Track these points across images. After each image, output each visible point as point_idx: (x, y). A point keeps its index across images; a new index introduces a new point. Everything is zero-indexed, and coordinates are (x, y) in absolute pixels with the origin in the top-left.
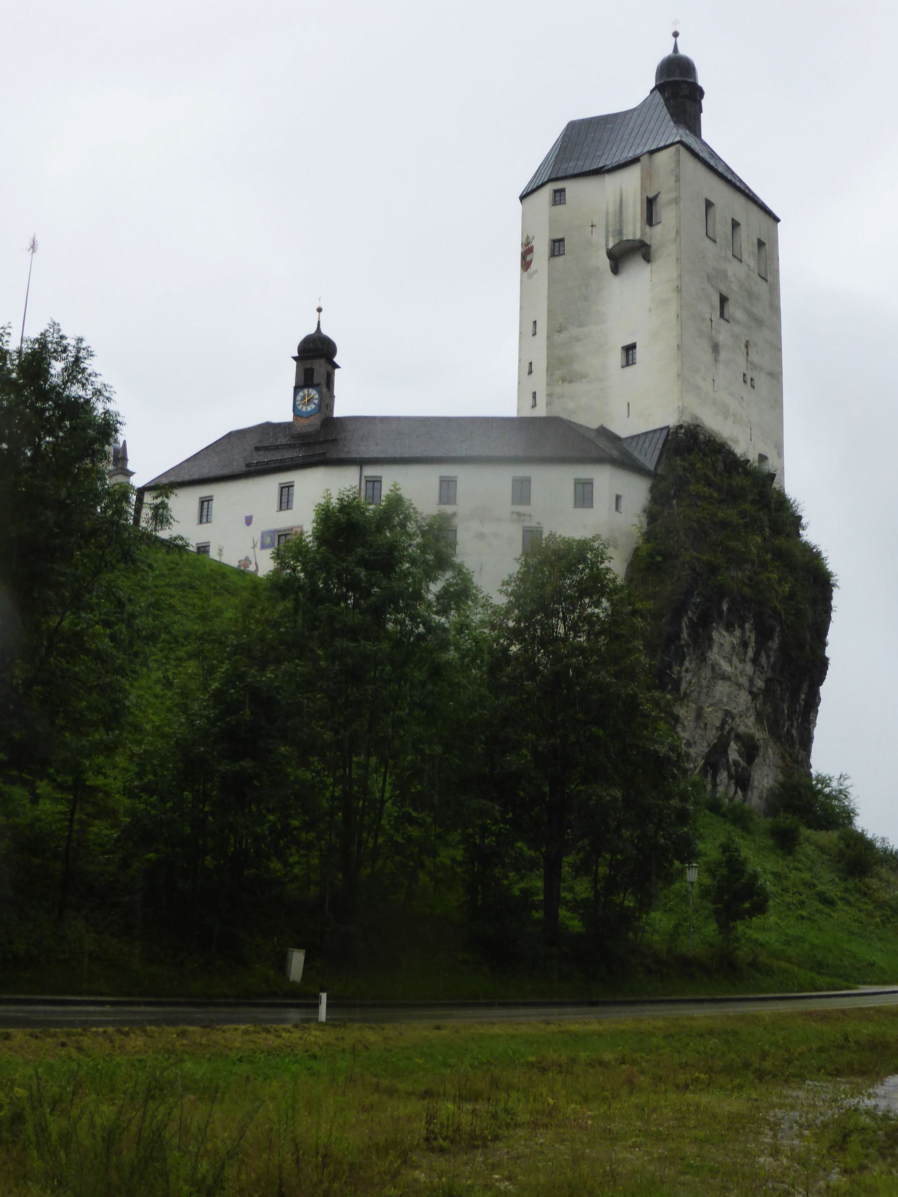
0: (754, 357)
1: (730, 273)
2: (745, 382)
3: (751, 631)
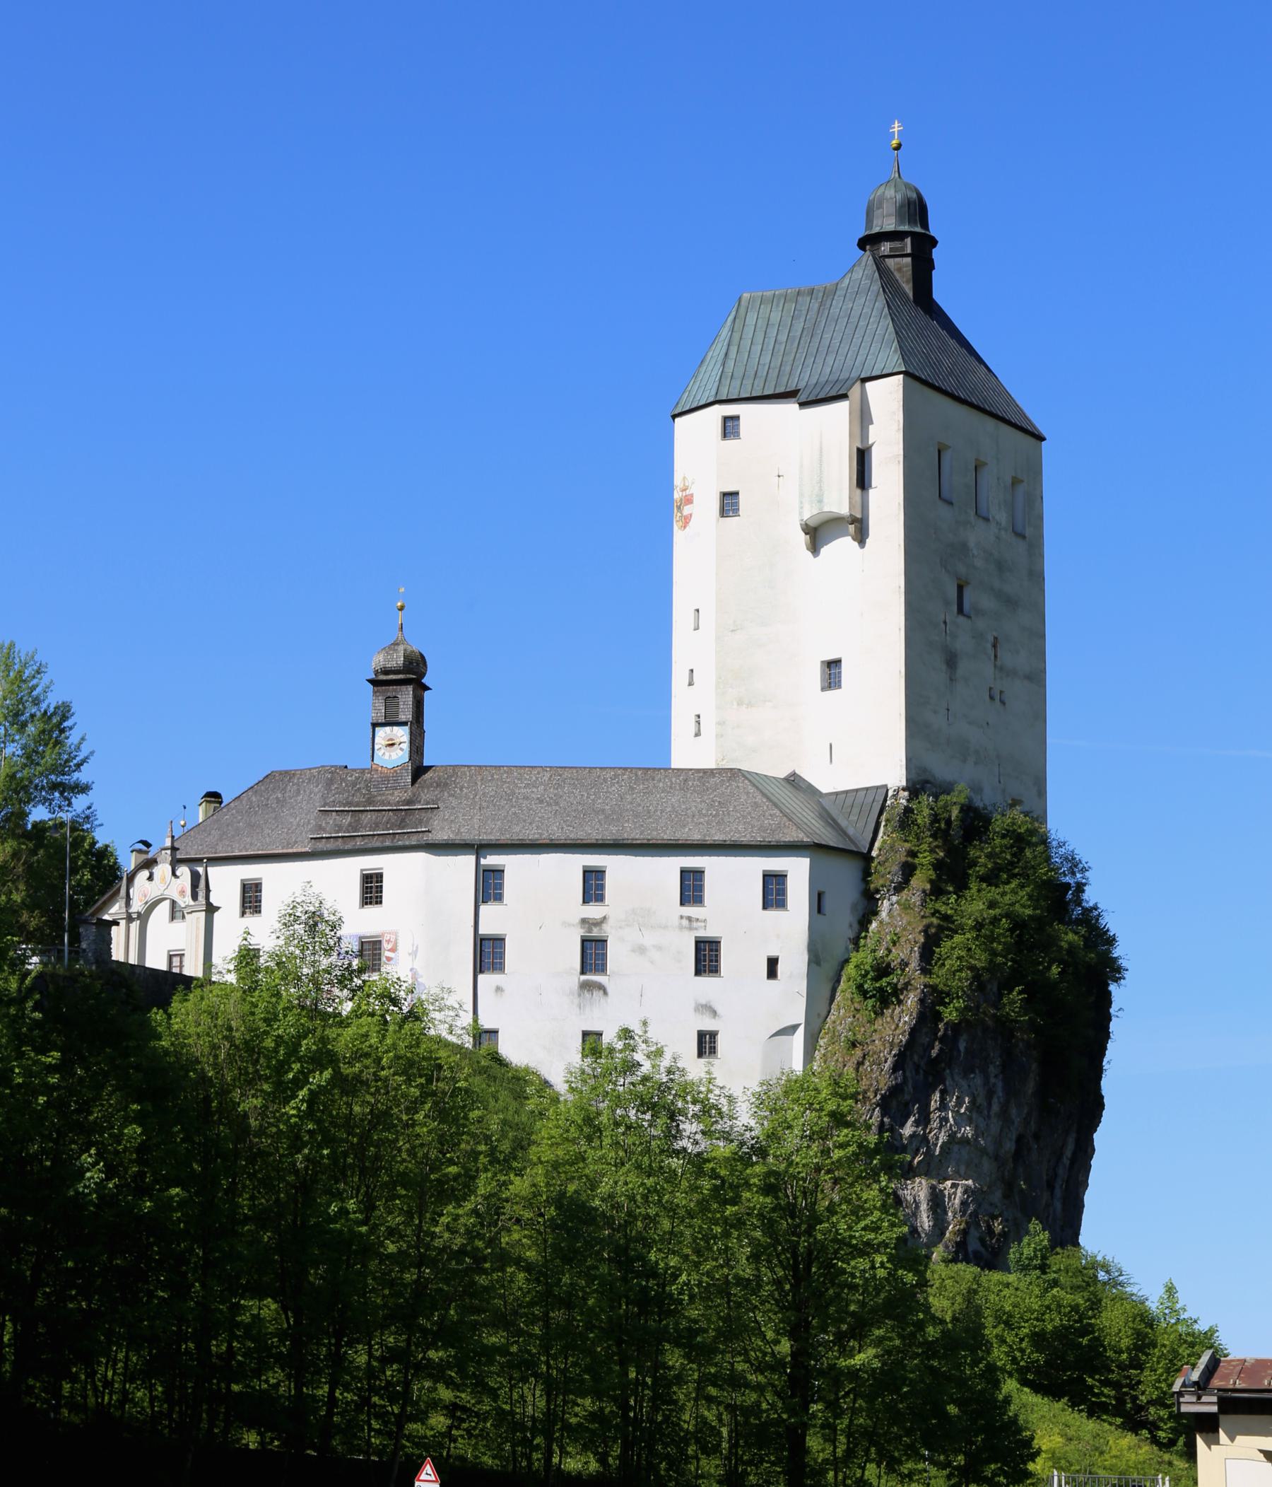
0: (1006, 658)
1: (972, 544)
2: (992, 698)
3: (996, 1076)
